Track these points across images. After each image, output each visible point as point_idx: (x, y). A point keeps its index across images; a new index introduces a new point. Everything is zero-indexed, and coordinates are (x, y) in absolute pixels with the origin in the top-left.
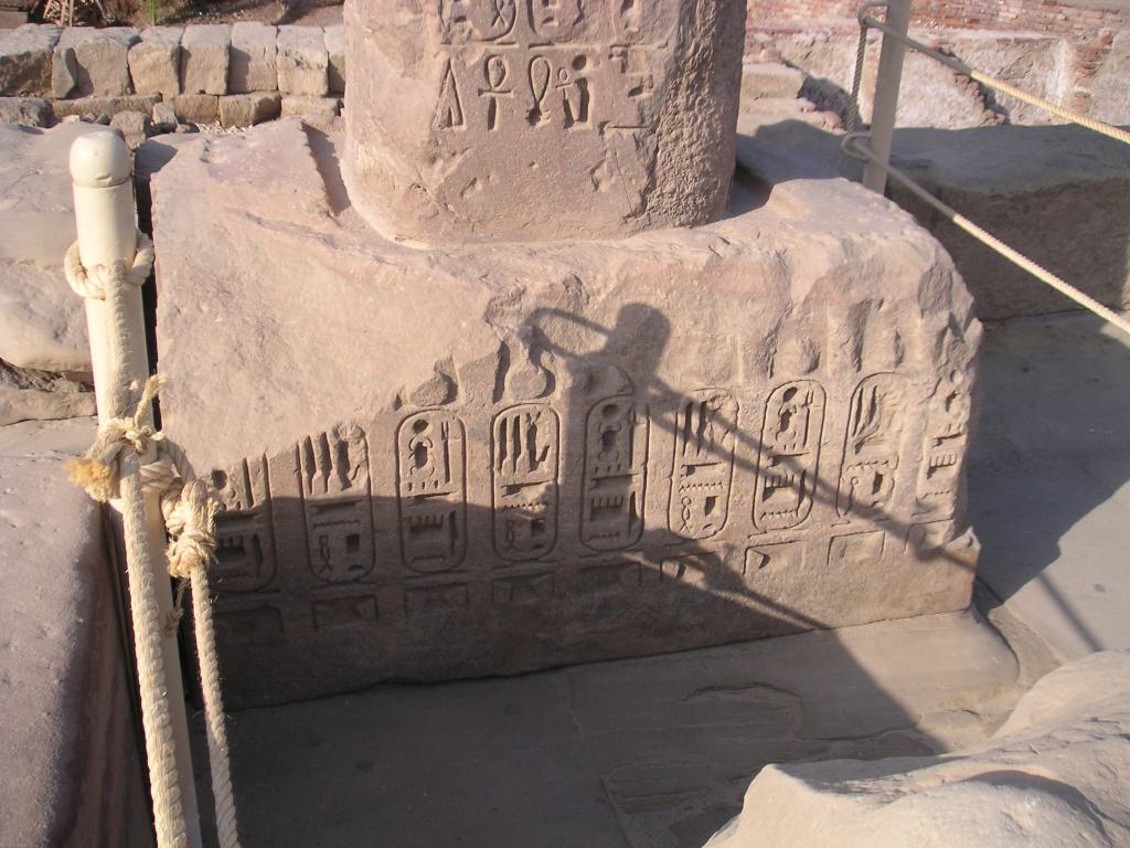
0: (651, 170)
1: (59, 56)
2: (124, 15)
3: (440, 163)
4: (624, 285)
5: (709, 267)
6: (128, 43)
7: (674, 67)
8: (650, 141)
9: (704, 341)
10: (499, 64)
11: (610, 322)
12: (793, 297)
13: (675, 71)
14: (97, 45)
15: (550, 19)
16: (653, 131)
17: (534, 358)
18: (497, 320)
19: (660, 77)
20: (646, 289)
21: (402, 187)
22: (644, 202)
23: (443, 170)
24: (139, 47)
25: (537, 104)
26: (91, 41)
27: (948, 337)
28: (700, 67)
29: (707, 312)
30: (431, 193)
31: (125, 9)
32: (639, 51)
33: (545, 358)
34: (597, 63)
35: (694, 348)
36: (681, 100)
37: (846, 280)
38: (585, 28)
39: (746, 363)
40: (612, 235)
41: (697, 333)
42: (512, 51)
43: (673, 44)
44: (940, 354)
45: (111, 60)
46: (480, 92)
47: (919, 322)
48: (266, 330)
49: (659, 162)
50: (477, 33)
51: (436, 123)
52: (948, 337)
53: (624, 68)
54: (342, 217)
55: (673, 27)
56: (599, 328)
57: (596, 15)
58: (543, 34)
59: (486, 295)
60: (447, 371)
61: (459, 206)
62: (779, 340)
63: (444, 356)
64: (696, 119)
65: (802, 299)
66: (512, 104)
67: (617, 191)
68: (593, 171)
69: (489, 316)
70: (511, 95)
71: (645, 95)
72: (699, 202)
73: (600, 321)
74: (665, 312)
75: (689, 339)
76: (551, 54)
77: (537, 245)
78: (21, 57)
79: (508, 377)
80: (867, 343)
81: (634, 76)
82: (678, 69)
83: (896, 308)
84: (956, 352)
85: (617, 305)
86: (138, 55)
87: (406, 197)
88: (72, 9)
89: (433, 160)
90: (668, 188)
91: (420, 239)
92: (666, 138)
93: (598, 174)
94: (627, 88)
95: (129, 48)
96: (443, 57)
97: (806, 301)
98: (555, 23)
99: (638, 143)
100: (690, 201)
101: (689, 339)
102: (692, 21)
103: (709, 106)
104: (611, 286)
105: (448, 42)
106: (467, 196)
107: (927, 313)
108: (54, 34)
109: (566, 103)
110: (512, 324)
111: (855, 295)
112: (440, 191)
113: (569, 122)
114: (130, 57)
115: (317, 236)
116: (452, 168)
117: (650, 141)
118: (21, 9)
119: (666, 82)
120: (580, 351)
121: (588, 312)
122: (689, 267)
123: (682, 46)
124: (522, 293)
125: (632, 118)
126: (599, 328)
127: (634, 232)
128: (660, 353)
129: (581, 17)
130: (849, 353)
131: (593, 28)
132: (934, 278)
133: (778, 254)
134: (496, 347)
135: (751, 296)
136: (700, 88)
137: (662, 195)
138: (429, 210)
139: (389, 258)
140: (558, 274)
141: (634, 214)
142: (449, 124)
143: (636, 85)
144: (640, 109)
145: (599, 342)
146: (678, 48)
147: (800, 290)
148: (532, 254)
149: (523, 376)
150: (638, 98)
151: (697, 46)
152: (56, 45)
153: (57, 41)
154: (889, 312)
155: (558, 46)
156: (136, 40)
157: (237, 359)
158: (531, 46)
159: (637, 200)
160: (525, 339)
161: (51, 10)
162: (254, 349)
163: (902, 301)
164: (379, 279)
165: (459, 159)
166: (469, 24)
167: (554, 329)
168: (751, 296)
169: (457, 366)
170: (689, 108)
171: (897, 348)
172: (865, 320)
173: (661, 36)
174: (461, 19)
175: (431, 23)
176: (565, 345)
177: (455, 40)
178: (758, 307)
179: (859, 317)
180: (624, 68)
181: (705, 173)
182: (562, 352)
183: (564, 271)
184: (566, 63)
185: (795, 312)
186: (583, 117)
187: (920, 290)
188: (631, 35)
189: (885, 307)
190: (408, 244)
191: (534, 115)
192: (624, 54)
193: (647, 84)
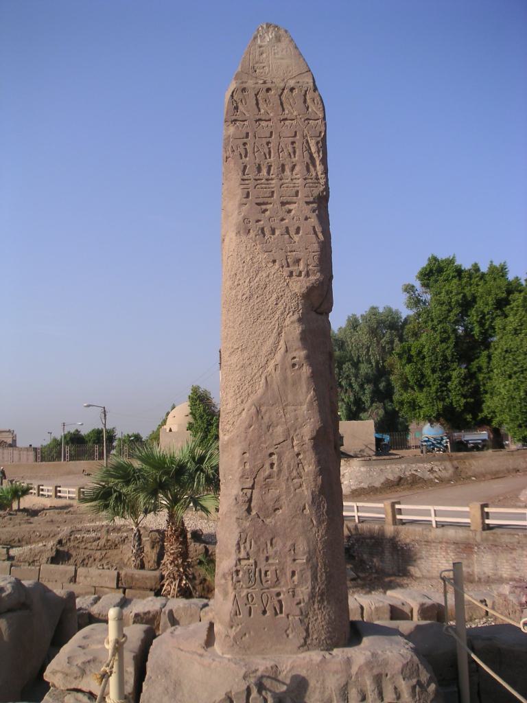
0: (307, 630)
1: (165, 613)
2: (206, 593)
3: (234, 628)
4: (292, 668)
5: (321, 662)
6: (201, 607)
7: (311, 595)
8: (306, 620)
9: (321, 688)
10: (252, 595)
11: (288, 681)
12: (352, 673)
13: (312, 596)
14: (185, 608)
15: (268, 581)
16: (307, 617)
17: (260, 692)
18: (248, 679)
19: (306, 599)
20: (299, 670)
21: (223, 636)
22: (305, 642)
23: (235, 630)
24: (207, 609)
25: (265, 608)
26: (181, 605)
27: (418, 689)
28: (322, 595)
29: (321, 678)
30: (232, 637)
31: (206, 590)
32: (298, 590)
33: (264, 693)
34: (284, 595)
35: (318, 691)
36: (316, 606)
37: (371, 666)
38: (279, 583)
39: (336, 697)
40: (295, 653)
41: (318, 685)
42: (255, 591)
43: (310, 588)
44: (415, 696)
45: (192, 616)
46: (246, 605)
47: (403, 682)
48: (177, 684)
49: (310, 627)
50: (244, 586)
51: (232, 615)
52: (418, 689)
53: (294, 596)
54: (209, 649)
55: (309, 583)
56: (284, 683)
57: (283, 579)
58: (265, 585)
59: (244, 670)
60: (230, 695)
61: (239, 643)
62: (349, 688)
63: (229, 690)
64: (323, 612)
65: (355, 673)
66: (257, 607)
67: (296, 638)
68: (286, 631)
69: (245, 677)
70: (256, 605)
71: (302, 605)
72: (328, 642)
73: (284, 681)
74: (306, 678)
75: (315, 688)
76: (269, 592)
77: (267, 657)
78: (145, 614)
79: (250, 699)
80: (384, 690)
81: (297, 599)
82: (313, 596)
83: (393, 677)
84: (424, 696)
85: (290, 675)
86: (206, 613)
87: (224, 640)
88: (176, 590)
89: (232, 627)
90: (315, 637)
91: (228, 654)
92: (312, 619)
93: (288, 632)
94: (295, 602)
95: (201, 609)
96: (234, 593)
97: (357, 674)
98: (269, 582)
99: (301, 621)
100: (325, 642)
101: (315, 688)
102: (317, 579)
103: (327, 608)
104: (288, 668)
105: (235, 589)
106: (243, 639)
107: (406, 679)
108: (164, 602)
109: (275, 609)
110: (252, 680)
111: (375, 671)
112: (234, 638)
113: (276, 614)
114: (201, 614)
115: (197, 654)
116: (238, 630)
117: (306, 620)
118: (151, 590)
119: (309, 600)
120: (277, 691)
121: (280, 678)
122: (314, 662)
123: (313, 588)
124: (256, 670)
125: (298, 612)
126: (284, 683)
127: (302, 652)
128: (305, 692)
129: (278, 580)
130: (376, 694)
131: (282, 583)
132: (409, 666)
133: (348, 658)
134: (245, 687)
135: (336, 672)
136: (323, 601)
137: (313, 639)
138: (231, 644)
139: (217, 659)
140: (269, 664)
141: (302, 646)
142: (236, 614)
143: (298, 601)
144: (301, 609)
145: (284, 688)
146: (312, 589)
147: (354, 669)
148: (264, 659)
149: (255, 699)
150: (300, 606)
151: (319, 588)
152: (164, 607)
153: (164, 606)
154: (390, 679)
155: (272, 589)
156: (206, 605)
157: (166, 692)
158: (262, 589)
159: (302, 641)
160: (256, 685)
161: (165, 590)
162: (172, 689)
163: (395, 674)
164: (213, 666)
165: (240, 626)
166: (241, 583)
167: (267, 683)
168: (336, 672)
169: (233, 694)
170: (319, 609)
171: (396, 693)
172: (381, 682)
173: (306, 585)
174: (239, 581)
175: (230, 583)
176: (272, 689)
177: (237, 589)
178: (338, 676)
179: (378, 680)
180: (294, 596)
181: (329, 632)
182: (270, 691)
183: (273, 663)
184: (274, 595)
185: (353, 678)
186: (281, 612)
187: (402, 670)
188: (295, 585)
189: (389, 677)
190: (225, 656)
191: (264, 612)
192: (293, 591)
193: (302, 601)
